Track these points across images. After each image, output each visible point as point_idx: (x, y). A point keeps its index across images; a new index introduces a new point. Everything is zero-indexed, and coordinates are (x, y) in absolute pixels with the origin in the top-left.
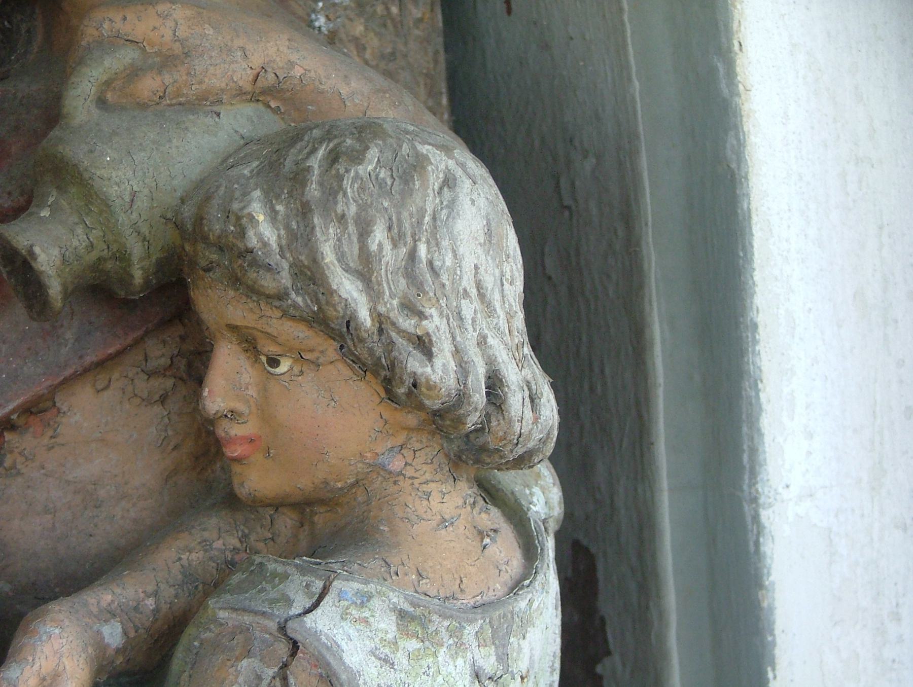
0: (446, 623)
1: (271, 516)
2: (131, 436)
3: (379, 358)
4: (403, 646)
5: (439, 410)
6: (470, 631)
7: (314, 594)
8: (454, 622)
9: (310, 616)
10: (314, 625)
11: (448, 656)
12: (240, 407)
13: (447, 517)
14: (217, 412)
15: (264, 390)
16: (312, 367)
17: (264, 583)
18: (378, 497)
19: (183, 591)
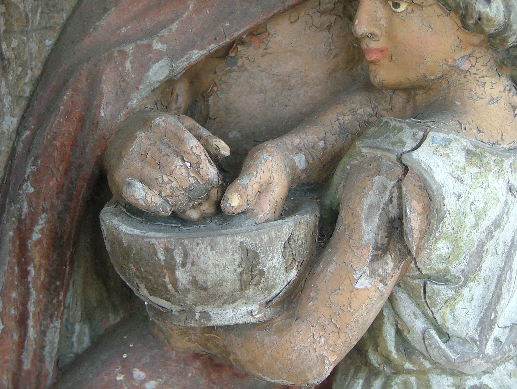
0: (494, 158)
1: (391, 96)
2: (310, 49)
3: (459, 3)
4: (468, 170)
5: (492, 34)
6: (507, 162)
7: (417, 139)
8: (498, 158)
9: (415, 152)
10: (417, 157)
11: (494, 177)
12: (376, 31)
13: (494, 97)
14: (363, 34)
15: (390, 22)
16: (419, 8)
17: (388, 133)
18: (454, 85)
19: (340, 137)
